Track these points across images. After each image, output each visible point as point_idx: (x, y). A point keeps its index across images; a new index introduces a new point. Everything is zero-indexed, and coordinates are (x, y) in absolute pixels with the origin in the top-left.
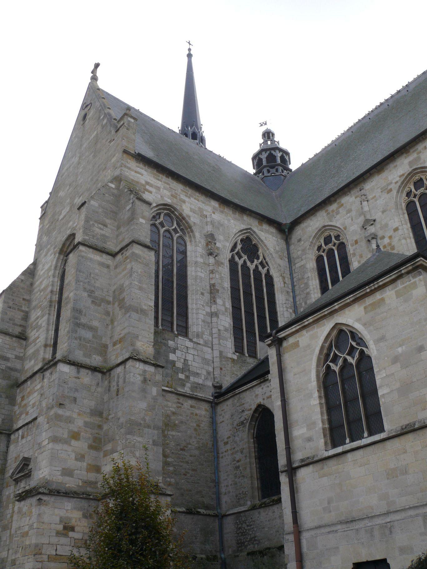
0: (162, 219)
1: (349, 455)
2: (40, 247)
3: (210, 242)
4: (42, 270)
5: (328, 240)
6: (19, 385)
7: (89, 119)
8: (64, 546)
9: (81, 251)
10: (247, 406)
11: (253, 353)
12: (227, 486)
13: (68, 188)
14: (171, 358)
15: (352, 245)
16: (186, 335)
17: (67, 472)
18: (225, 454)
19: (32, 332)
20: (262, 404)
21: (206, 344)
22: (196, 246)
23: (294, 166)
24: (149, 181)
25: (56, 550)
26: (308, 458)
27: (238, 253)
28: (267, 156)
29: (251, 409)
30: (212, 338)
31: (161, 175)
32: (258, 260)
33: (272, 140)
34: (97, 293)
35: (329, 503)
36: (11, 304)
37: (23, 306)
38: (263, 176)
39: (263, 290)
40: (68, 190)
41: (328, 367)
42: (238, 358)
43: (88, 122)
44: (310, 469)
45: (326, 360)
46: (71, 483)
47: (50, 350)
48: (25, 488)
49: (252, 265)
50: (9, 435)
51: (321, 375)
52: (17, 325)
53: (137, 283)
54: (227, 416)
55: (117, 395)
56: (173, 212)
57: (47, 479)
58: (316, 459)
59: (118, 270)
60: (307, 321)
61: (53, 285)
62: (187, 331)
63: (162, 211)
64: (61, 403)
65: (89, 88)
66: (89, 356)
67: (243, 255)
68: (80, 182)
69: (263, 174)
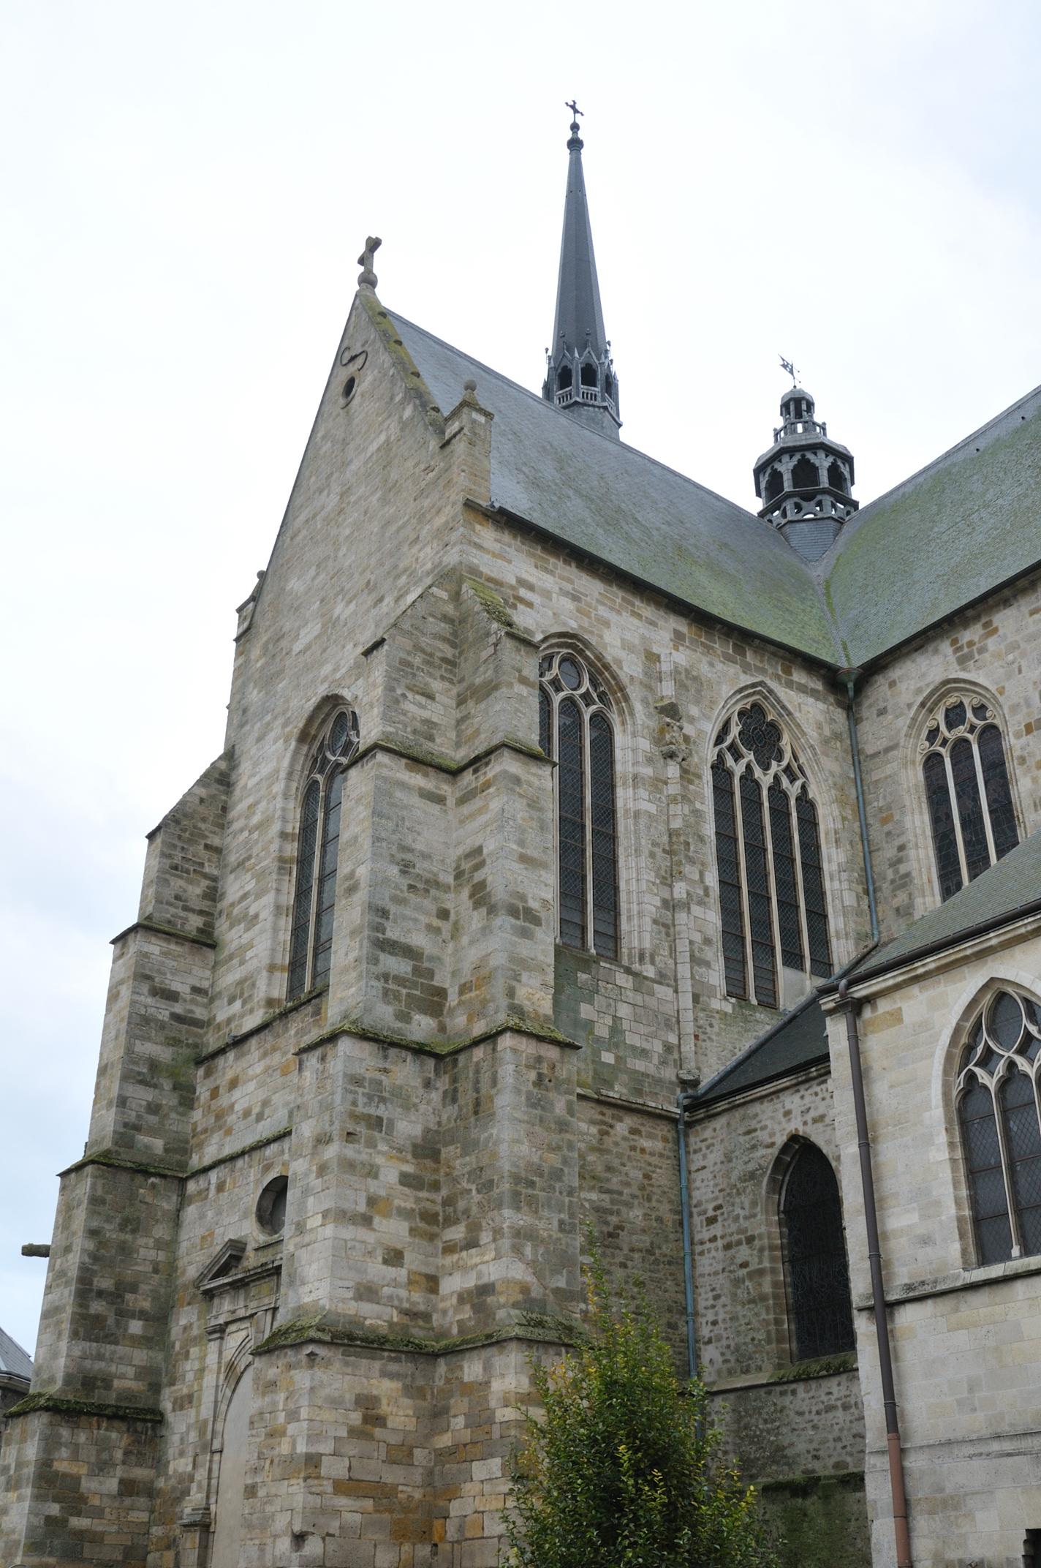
0: (555, 670)
1: (1020, 1286)
2: (239, 713)
3: (668, 725)
4: (253, 775)
5: (956, 714)
6: (206, 1060)
7: (362, 395)
8: (365, 1460)
9: (380, 765)
10: (763, 1136)
11: (769, 1000)
12: (715, 1323)
13: (312, 572)
14: (583, 1016)
15: (1018, 736)
16: (615, 957)
17: (367, 1292)
18: (708, 1245)
19: (233, 931)
20: (801, 1133)
21: (661, 978)
22: (634, 735)
23: (865, 491)
24: (525, 576)
25: (350, 1469)
26: (923, 1283)
27: (733, 748)
28: (795, 466)
29: (773, 1144)
30: (676, 964)
31: (552, 560)
32: (779, 761)
33: (806, 422)
34: (421, 867)
35: (971, 1390)
36: (177, 860)
37: (206, 864)
38: (784, 521)
39: (791, 839)
40: (314, 579)
41: (972, 1077)
42: (734, 1010)
43: (361, 405)
44: (928, 1308)
45: (966, 1060)
46: (376, 1317)
47: (282, 980)
48: (234, 1312)
49: (765, 775)
50: (183, 1181)
51: (955, 1093)
52: (193, 911)
53: (515, 847)
54: (715, 1157)
55: (476, 1113)
56: (581, 652)
57: (323, 1308)
58: (940, 1287)
59: (466, 809)
60: (923, 965)
61: (284, 819)
62: (616, 946)
63: (557, 650)
64: (351, 1130)
65: (357, 308)
66: (404, 1017)
67: (743, 750)
68: (347, 564)
69: (784, 515)
